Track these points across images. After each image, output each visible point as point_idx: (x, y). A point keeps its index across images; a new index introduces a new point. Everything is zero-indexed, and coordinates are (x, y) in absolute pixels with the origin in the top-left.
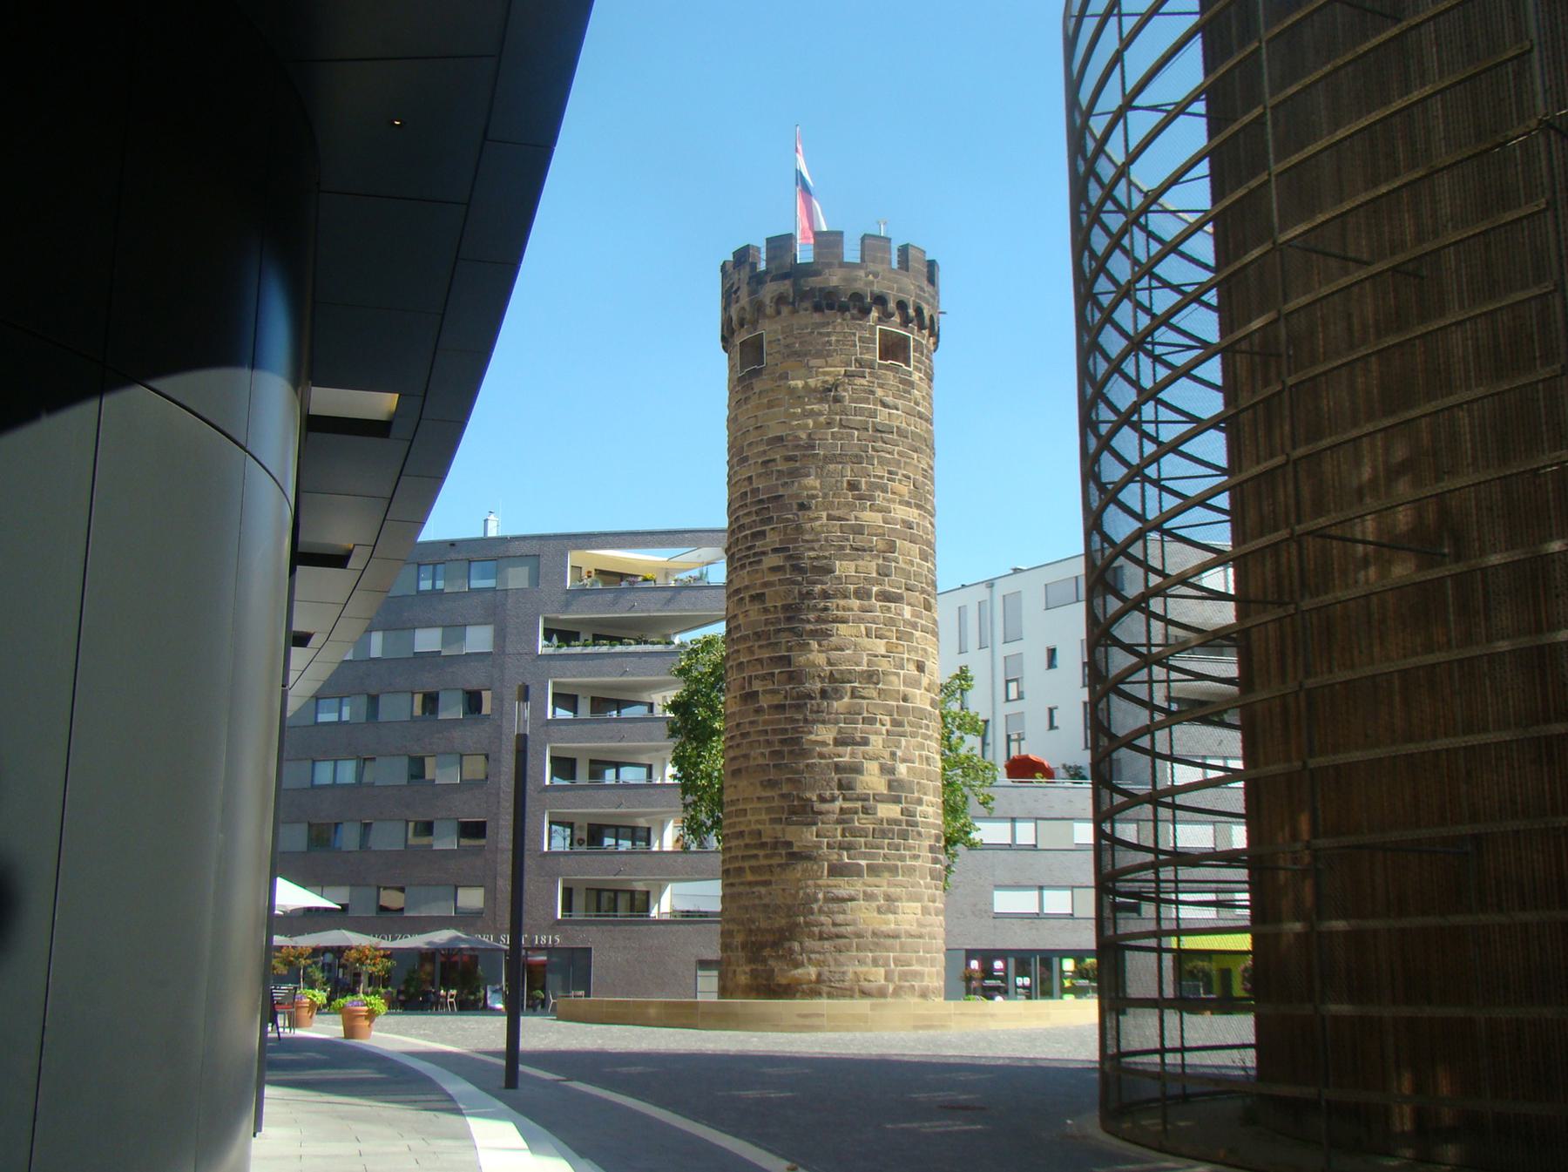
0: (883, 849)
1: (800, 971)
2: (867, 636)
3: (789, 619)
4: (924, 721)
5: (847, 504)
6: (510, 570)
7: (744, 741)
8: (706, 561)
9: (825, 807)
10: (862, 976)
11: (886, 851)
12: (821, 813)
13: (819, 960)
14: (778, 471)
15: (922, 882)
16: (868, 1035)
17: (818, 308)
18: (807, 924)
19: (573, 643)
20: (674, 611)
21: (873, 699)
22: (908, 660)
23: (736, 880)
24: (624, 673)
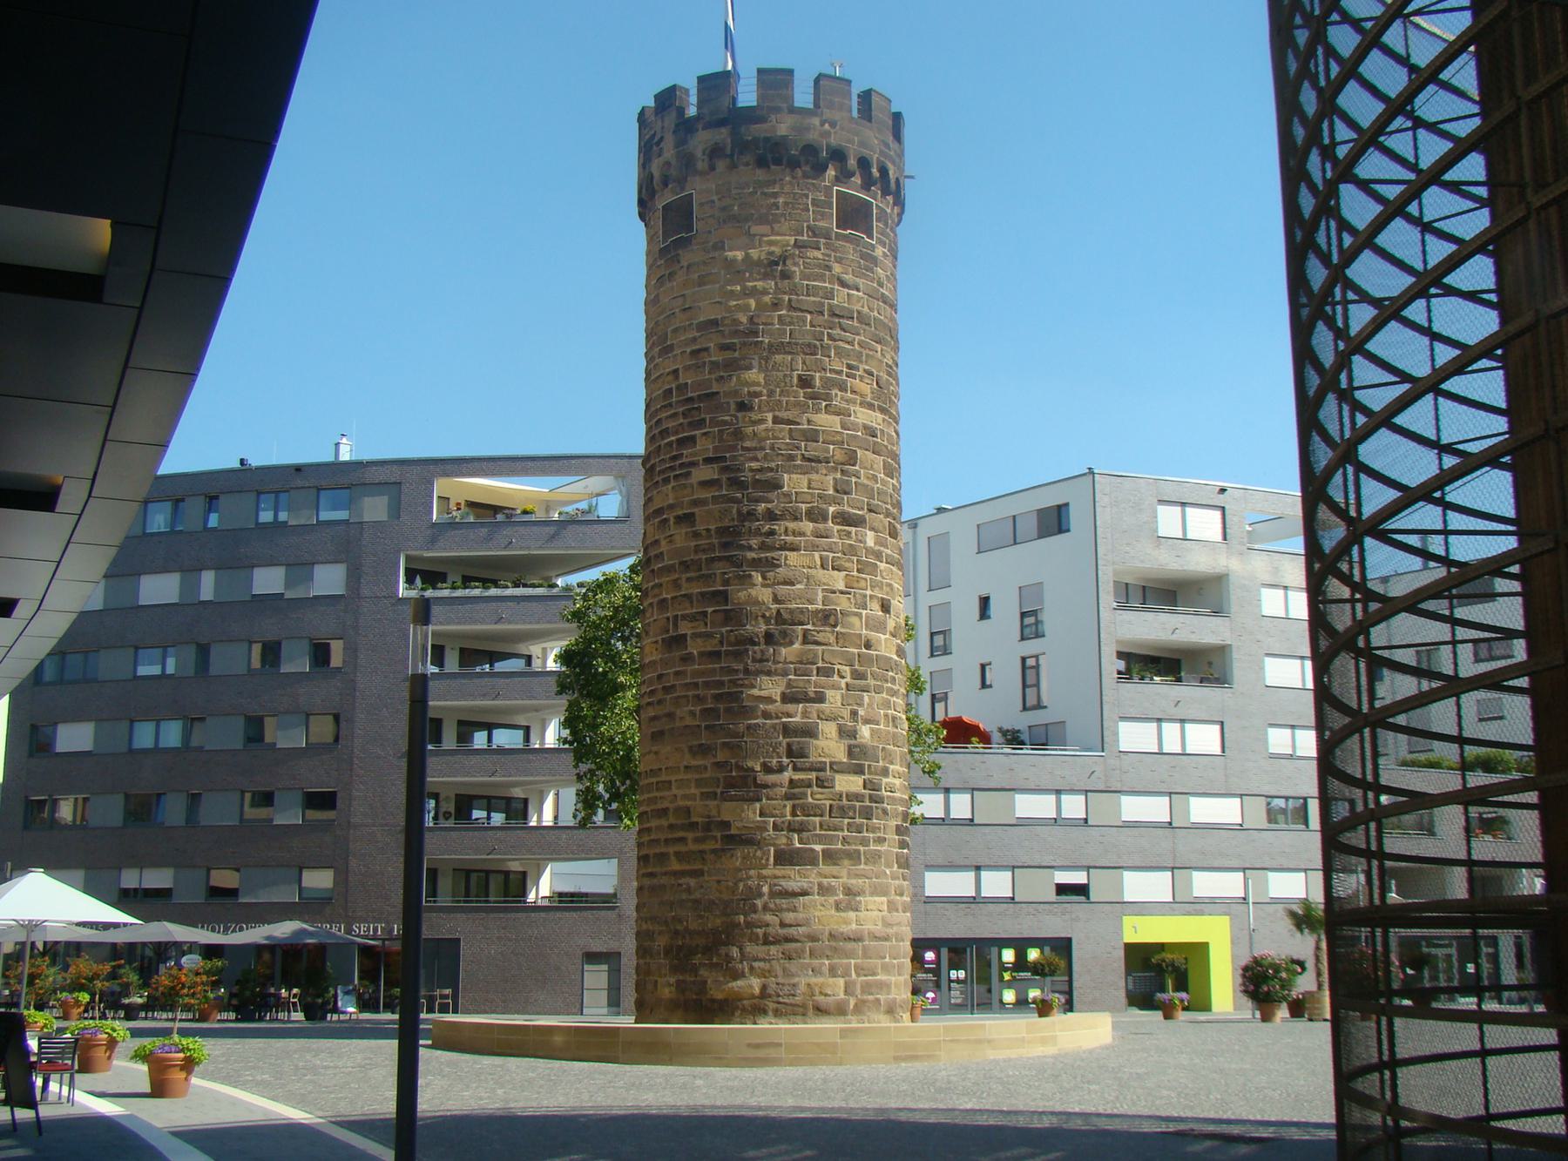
0: (843, 830)
1: (739, 983)
2: (823, 567)
3: (725, 546)
4: (890, 673)
5: (797, 404)
6: (366, 499)
7: (668, 697)
8: (594, 492)
9: (772, 778)
10: (817, 991)
11: (846, 833)
12: (766, 786)
13: (763, 970)
14: (712, 363)
15: (888, 872)
16: (840, 1069)
17: (762, 163)
18: (749, 925)
19: (439, 585)
20: (558, 548)
21: (830, 644)
22: (871, 596)
23: (658, 869)
24: (500, 620)
